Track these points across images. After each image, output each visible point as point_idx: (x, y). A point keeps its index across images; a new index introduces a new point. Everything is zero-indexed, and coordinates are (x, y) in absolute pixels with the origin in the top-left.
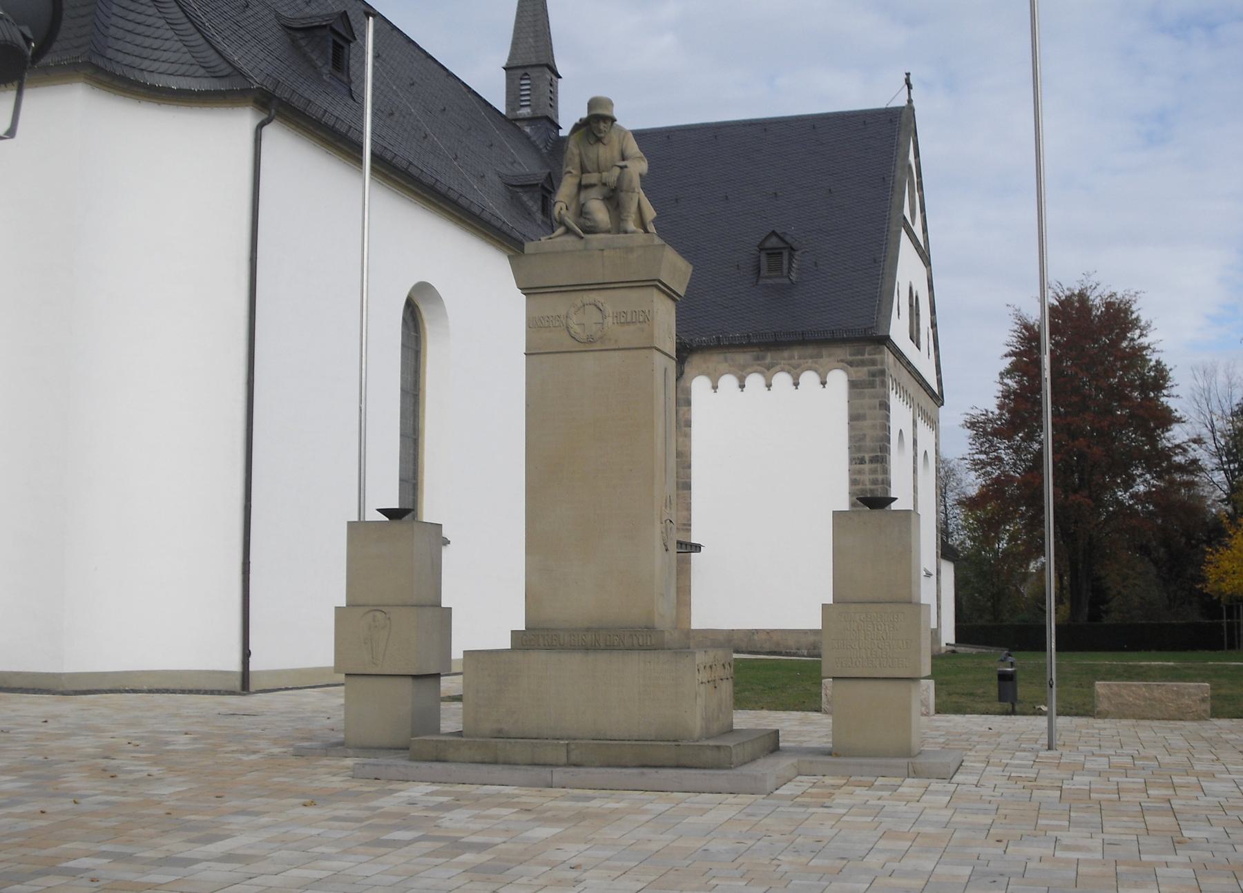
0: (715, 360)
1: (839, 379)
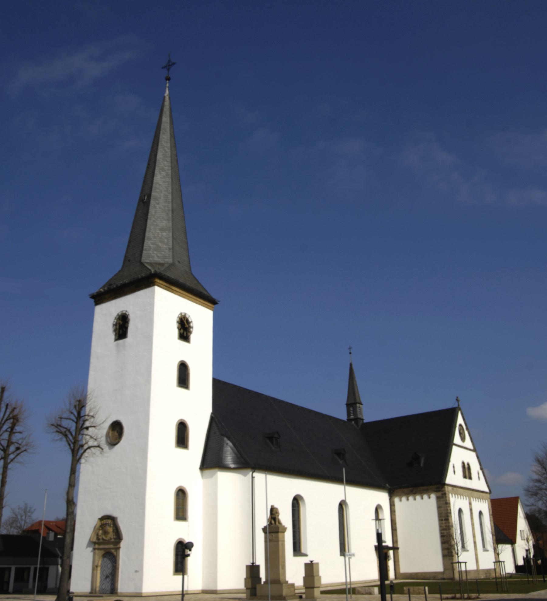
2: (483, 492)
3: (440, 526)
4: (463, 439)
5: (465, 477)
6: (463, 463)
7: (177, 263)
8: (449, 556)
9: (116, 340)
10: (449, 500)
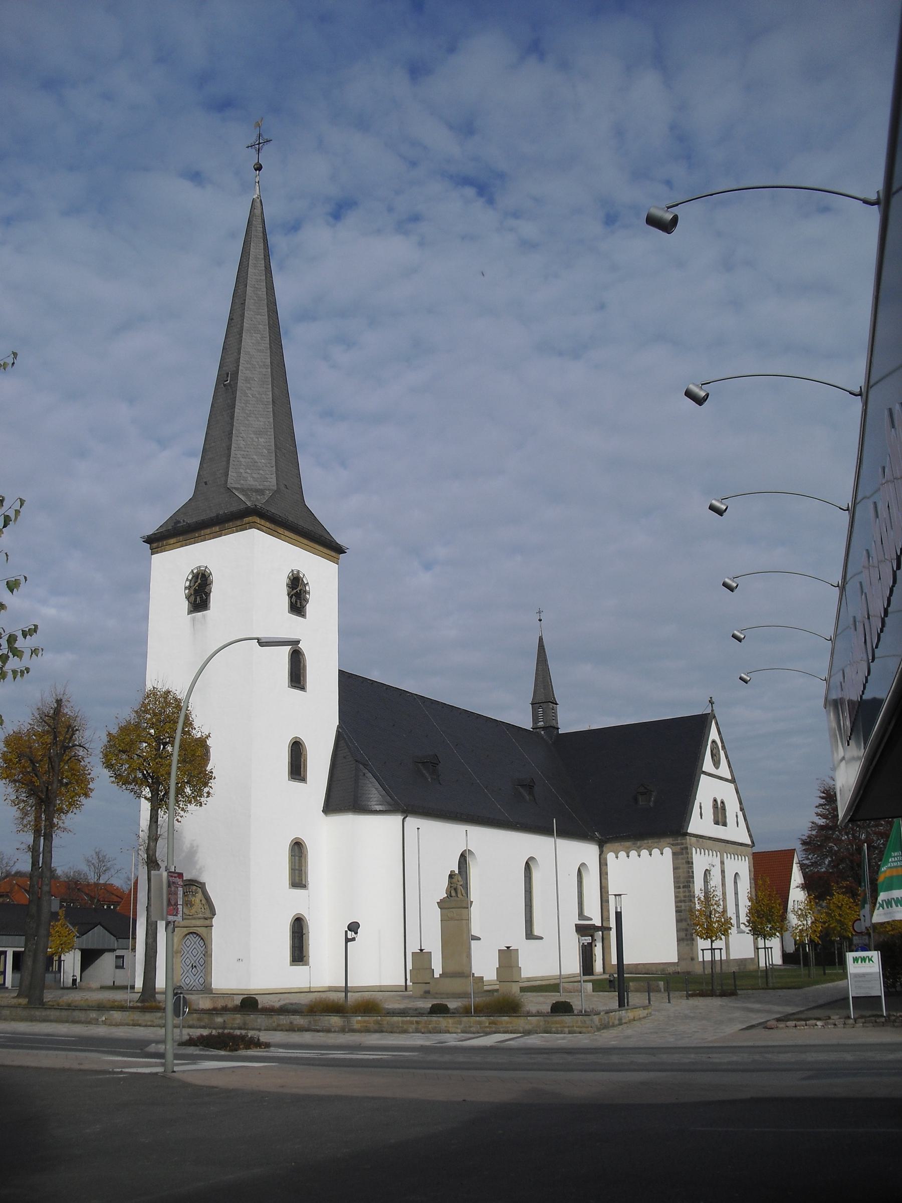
0: (616, 845)
1: (668, 851)
2: (742, 844)
3: (676, 897)
4: (717, 764)
5: (717, 823)
6: (715, 800)
8: (687, 940)
9: (190, 612)
10: (692, 858)
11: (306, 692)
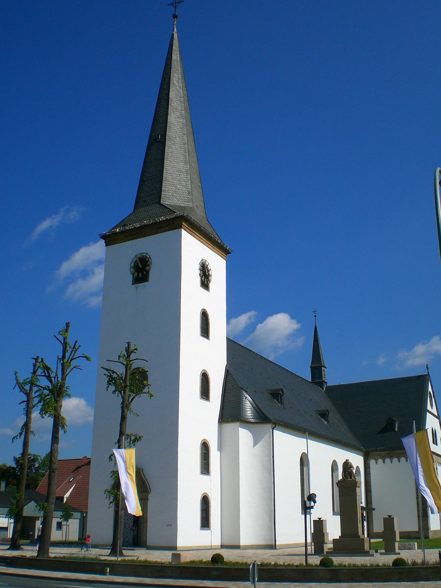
7: (195, 207)
11: (209, 340)
